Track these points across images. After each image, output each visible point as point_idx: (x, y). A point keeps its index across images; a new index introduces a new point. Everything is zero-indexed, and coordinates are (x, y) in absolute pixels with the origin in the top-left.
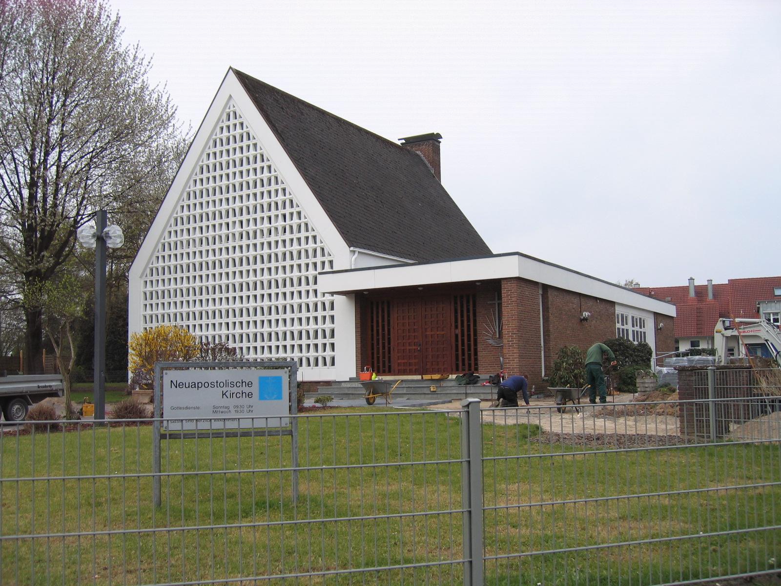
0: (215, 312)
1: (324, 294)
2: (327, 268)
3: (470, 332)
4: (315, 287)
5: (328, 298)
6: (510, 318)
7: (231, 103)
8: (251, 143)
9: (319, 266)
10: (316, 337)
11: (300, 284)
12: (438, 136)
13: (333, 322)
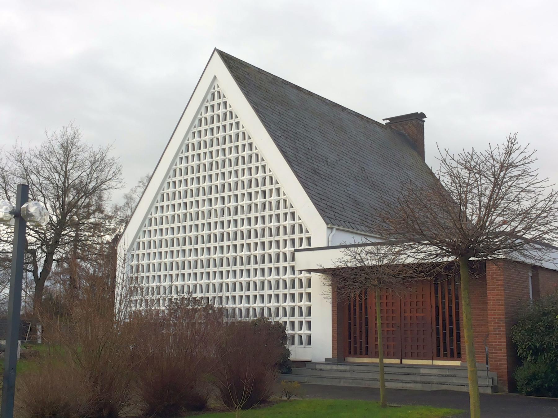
0: (196, 286)
1: (301, 271)
2: (305, 246)
3: (449, 317)
4: (292, 264)
5: (304, 275)
6: (496, 303)
7: (216, 84)
8: (259, 164)
9: (297, 243)
10: (293, 315)
11: (278, 261)
12: (423, 115)
13: (310, 300)
